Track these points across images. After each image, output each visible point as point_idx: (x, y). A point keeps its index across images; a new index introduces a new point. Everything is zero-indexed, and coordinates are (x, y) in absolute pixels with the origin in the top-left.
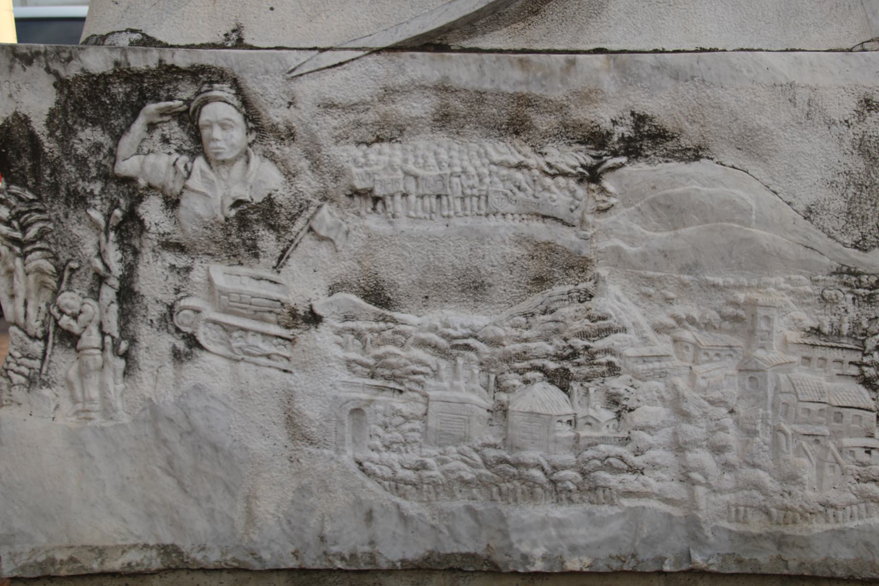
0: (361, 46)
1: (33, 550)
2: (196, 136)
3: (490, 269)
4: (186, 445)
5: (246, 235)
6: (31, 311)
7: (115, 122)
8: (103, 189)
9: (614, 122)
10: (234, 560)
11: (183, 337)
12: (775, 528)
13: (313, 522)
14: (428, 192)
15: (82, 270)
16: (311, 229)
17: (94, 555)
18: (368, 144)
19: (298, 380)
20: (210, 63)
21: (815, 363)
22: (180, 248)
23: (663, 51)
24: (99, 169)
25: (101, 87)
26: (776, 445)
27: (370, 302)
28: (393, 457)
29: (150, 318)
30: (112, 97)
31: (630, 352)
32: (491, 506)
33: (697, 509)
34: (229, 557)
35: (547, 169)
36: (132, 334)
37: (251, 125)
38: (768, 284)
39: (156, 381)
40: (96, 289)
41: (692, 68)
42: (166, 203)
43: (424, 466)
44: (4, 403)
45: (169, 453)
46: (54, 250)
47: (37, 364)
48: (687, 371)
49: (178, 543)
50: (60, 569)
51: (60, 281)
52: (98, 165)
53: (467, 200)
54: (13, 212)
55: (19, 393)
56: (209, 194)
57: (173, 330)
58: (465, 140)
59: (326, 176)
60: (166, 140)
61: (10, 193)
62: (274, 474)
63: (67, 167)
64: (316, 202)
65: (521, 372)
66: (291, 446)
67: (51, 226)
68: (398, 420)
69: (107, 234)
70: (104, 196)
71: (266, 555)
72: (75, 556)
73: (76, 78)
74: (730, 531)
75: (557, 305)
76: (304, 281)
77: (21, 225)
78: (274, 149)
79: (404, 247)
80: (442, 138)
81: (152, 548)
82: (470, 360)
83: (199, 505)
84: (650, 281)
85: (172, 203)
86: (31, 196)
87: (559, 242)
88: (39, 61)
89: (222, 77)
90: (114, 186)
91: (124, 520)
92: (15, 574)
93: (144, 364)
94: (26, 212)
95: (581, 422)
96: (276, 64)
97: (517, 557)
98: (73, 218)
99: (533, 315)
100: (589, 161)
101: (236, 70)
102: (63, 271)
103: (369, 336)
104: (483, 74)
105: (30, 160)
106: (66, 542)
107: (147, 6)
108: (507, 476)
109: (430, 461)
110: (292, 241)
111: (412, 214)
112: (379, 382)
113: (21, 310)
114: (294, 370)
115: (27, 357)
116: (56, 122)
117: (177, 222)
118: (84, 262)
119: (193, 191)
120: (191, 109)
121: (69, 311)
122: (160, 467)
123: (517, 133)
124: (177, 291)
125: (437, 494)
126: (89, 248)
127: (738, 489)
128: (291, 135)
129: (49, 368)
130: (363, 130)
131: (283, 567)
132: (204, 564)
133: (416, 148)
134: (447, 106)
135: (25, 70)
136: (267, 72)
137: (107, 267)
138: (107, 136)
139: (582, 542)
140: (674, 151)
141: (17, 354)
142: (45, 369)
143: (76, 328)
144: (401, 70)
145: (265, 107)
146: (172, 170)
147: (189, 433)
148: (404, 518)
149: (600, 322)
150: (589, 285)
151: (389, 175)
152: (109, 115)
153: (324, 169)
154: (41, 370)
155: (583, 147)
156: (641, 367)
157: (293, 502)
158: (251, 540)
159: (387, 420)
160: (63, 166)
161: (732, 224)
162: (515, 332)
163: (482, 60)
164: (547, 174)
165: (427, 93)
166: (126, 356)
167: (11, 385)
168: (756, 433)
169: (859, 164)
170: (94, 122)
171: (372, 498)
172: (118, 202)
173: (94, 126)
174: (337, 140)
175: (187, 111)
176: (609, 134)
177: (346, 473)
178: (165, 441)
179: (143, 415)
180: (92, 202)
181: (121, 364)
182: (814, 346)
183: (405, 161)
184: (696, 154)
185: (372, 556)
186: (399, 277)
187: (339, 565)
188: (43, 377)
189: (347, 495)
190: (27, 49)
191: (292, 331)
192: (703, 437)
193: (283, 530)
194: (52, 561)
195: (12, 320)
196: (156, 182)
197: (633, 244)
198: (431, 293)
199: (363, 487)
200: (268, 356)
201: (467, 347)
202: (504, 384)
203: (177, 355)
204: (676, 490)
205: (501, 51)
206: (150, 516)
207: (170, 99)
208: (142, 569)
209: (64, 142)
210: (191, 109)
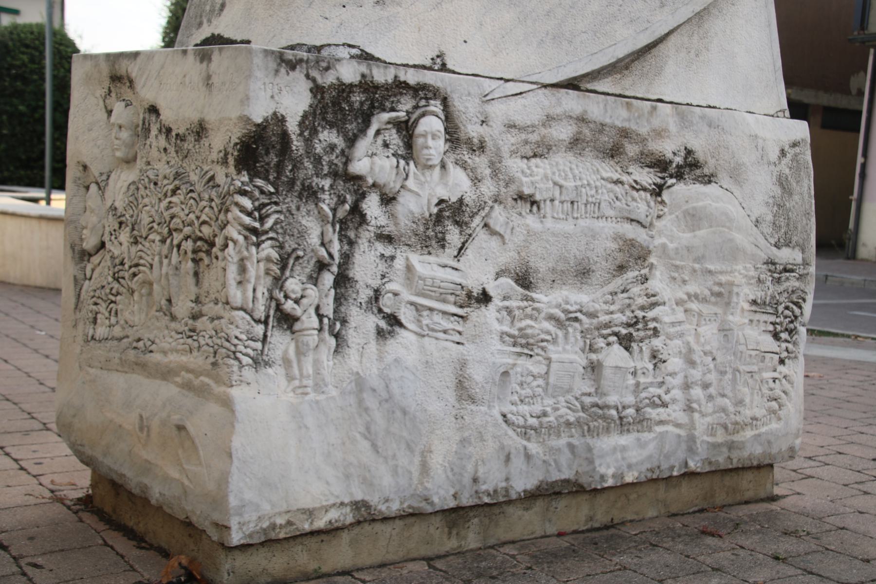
0: (534, 80)
1: (259, 517)
2: (409, 144)
3: (596, 259)
4: (377, 410)
5: (439, 229)
6: (259, 295)
7: (349, 126)
8: (331, 186)
9: (674, 154)
10: (410, 507)
11: (384, 317)
12: (729, 438)
13: (470, 468)
14: (567, 199)
15: (305, 258)
16: (486, 225)
17: (305, 517)
18: (528, 158)
19: (469, 350)
20: (432, 82)
21: (755, 323)
22: (389, 239)
23: (691, 105)
24: (330, 167)
25: (345, 95)
26: (734, 381)
27: (519, 285)
28: (524, 409)
29: (359, 301)
30: (351, 105)
31: (666, 319)
32: (583, 440)
33: (695, 429)
34: (405, 505)
35: (635, 185)
36: (343, 315)
37: (447, 137)
38: (736, 270)
39: (362, 357)
40: (315, 276)
41: (718, 119)
42: (382, 200)
43: (545, 414)
44: (234, 383)
45: (368, 419)
46: (281, 239)
47: (259, 345)
48: (694, 332)
49: (367, 498)
50: (280, 532)
51: (283, 269)
52: (331, 163)
53: (588, 206)
54: (257, 204)
55: (248, 373)
56: (421, 193)
57: (376, 311)
58: (583, 159)
59: (501, 183)
60: (386, 145)
61: (254, 186)
62: (444, 431)
63: (306, 164)
64: (490, 203)
65: (605, 337)
66: (457, 405)
67: (282, 217)
68: (531, 378)
69: (333, 225)
70: (332, 192)
71: (436, 500)
72: (291, 519)
73: (332, 86)
74: (708, 443)
75: (631, 285)
76: (479, 267)
77: (260, 215)
78: (466, 158)
79: (548, 241)
80: (570, 156)
81: (346, 505)
82: (575, 329)
83: (387, 463)
84: (677, 267)
85: (388, 200)
86: (272, 190)
87: (638, 240)
88: (301, 67)
89: (435, 95)
90: (342, 183)
91: (328, 483)
92: (242, 542)
93: (353, 342)
94: (268, 204)
95: (639, 372)
96: (476, 88)
97: (597, 478)
98: (303, 210)
99: (616, 293)
100: (659, 181)
101: (449, 90)
102: (287, 259)
103: (517, 313)
104: (606, 111)
105: (276, 156)
106: (284, 508)
107: (361, 26)
108: (598, 417)
109: (549, 409)
110: (470, 235)
111: (555, 215)
112: (518, 349)
113: (250, 294)
114: (465, 342)
115: (251, 339)
116: (307, 123)
117: (392, 216)
118: (308, 250)
119: (410, 190)
120: (412, 120)
121: (293, 296)
122: (360, 433)
123: (612, 157)
124: (383, 276)
125: (550, 434)
126: (314, 239)
127: (714, 412)
128: (482, 147)
129: (269, 350)
130: (528, 147)
131: (446, 507)
132: (387, 514)
133: (557, 163)
134: (580, 133)
135: (288, 74)
136: (469, 94)
137: (331, 256)
138: (341, 138)
139: (634, 461)
140: (699, 177)
141: (244, 337)
142: (266, 349)
143: (298, 311)
144: (559, 103)
145: (464, 123)
146: (395, 171)
147: (387, 401)
148: (528, 457)
149: (652, 299)
150: (645, 271)
151: (544, 184)
152: (345, 120)
153: (501, 177)
154: (262, 351)
155: (652, 170)
156: (672, 330)
157: (456, 452)
158: (426, 488)
159: (523, 379)
160: (303, 163)
161: (724, 229)
162: (605, 307)
163: (607, 100)
164: (633, 188)
165: (571, 122)
166: (337, 336)
167: (241, 366)
168: (726, 372)
169: (778, 191)
170: (331, 125)
171: (511, 443)
172: (345, 197)
173: (331, 128)
174: (513, 153)
175: (407, 122)
176: (671, 162)
177: (496, 425)
178: (366, 409)
179: (349, 387)
180: (323, 196)
181: (333, 342)
182: (756, 312)
183: (554, 173)
184: (708, 179)
185: (507, 490)
186: (541, 266)
187: (486, 500)
188: (265, 358)
189: (495, 442)
190: (293, 55)
191: (466, 310)
192: (699, 378)
193: (447, 477)
194: (273, 526)
195: (239, 305)
196: (381, 181)
197: (672, 242)
198: (558, 278)
199: (506, 435)
200: (445, 332)
201: (576, 319)
202: (596, 347)
203: (380, 333)
204: (682, 417)
205: (608, 94)
206: (347, 477)
207: (393, 110)
208: (339, 524)
209: (309, 142)
210: (412, 120)
